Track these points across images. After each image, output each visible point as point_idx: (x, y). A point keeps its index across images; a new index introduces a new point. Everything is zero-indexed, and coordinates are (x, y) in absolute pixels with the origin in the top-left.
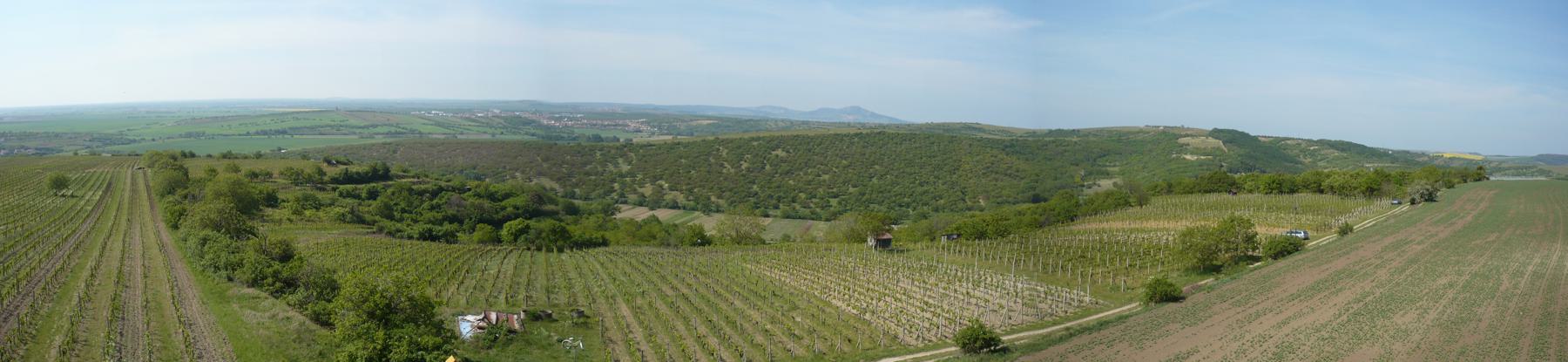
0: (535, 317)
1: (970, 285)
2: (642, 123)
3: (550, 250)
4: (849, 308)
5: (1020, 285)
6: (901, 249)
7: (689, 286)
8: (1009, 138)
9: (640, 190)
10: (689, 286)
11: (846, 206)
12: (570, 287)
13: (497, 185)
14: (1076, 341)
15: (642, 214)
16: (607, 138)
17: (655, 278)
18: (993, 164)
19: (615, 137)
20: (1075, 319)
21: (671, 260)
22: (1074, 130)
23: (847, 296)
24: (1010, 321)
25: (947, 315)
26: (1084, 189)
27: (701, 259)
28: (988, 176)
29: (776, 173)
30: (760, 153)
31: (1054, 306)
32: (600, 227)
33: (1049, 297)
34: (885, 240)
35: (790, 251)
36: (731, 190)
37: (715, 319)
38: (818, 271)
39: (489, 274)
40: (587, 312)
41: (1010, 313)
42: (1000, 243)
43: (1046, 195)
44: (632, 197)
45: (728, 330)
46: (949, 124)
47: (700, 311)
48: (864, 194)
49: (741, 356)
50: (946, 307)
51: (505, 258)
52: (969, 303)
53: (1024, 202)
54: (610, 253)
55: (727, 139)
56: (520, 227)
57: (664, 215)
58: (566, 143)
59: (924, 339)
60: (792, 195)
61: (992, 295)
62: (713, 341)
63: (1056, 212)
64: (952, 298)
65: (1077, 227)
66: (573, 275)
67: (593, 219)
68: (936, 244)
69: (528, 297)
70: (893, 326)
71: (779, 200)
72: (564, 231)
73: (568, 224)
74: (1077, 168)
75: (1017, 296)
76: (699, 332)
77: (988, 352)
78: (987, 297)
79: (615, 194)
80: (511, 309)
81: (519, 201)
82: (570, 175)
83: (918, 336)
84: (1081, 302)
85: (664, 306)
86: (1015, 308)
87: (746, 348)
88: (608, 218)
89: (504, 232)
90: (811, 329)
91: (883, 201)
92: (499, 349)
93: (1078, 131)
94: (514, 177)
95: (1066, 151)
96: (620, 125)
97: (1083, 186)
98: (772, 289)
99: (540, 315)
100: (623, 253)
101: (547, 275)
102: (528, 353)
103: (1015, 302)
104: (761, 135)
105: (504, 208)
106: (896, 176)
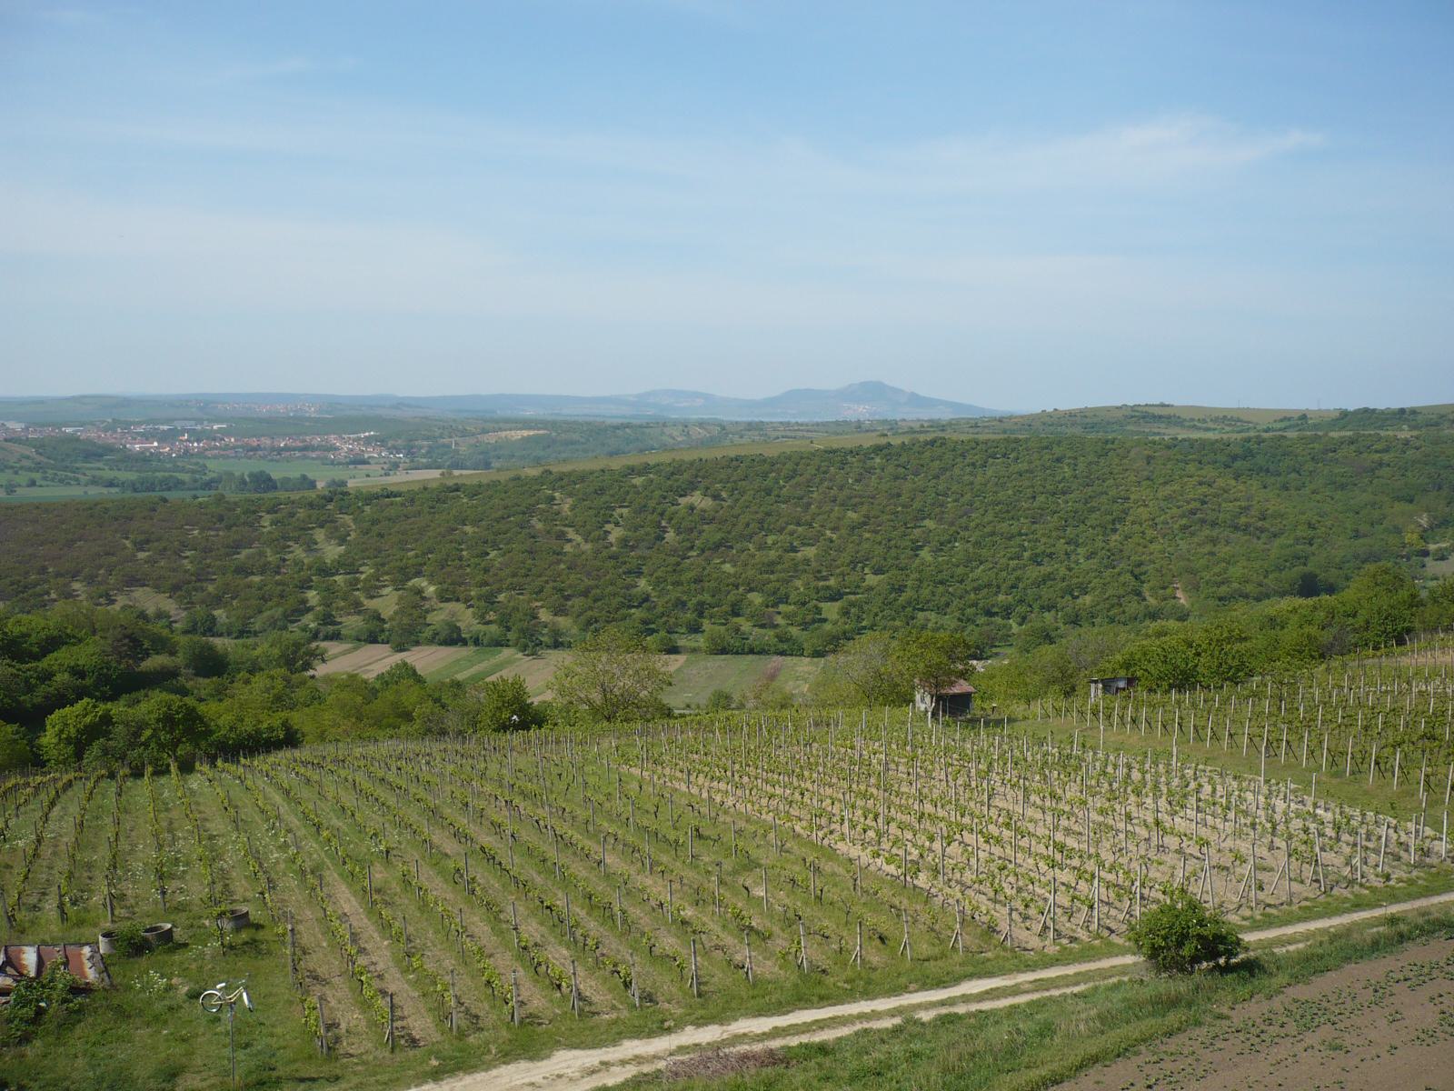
0: (135, 946)
1: (1163, 803)
2: (368, 441)
3: (161, 771)
4: (879, 861)
5: (1280, 805)
6: (995, 716)
7: (497, 826)
8: (1239, 436)
9: (370, 604)
10: (497, 826)
11: (859, 619)
12: (214, 856)
13: (24, 617)
14: (1414, 953)
15: (376, 662)
16: (287, 480)
17: (413, 815)
18: (1204, 503)
19: (304, 477)
20: (1411, 897)
21: (451, 768)
22: (1402, 411)
23: (871, 834)
24: (1261, 895)
25: (1111, 877)
26: (1428, 561)
27: (522, 762)
28: (1192, 534)
29: (692, 548)
30: (652, 504)
31: (1356, 861)
32: (279, 701)
33: (1345, 837)
34: (955, 696)
35: (731, 730)
36: (585, 594)
37: (560, 900)
38: (801, 777)
39: (13, 850)
40: (256, 915)
41: (1262, 876)
42: (1229, 698)
43: (1332, 575)
44: (352, 623)
45: (593, 926)
46: (1096, 411)
47: (523, 886)
48: (901, 589)
49: (627, 985)
50: (1108, 858)
51: (53, 804)
52: (1161, 848)
53: (1283, 594)
54: (305, 764)
55: (570, 474)
56: (88, 719)
57: (428, 660)
58: (187, 495)
59: (1058, 934)
60: (731, 598)
61: (1214, 828)
62: (558, 956)
63: (1360, 621)
64: (1122, 836)
65: (1414, 658)
66: (218, 825)
67: (259, 681)
68: (1077, 702)
69: (116, 899)
70: (984, 904)
71: (701, 610)
72: (192, 717)
73: (201, 700)
74: (1411, 507)
75: (1274, 833)
76: (525, 936)
77: (1211, 971)
78: (1204, 832)
79: (310, 616)
80: (75, 934)
81: (85, 654)
82: (201, 576)
83: (1045, 928)
84: (1426, 853)
85: (438, 880)
86: (1270, 862)
87: (638, 967)
88: (295, 678)
89: (48, 739)
90: (791, 914)
91: (947, 605)
92: (51, 1039)
93: (1414, 412)
94: (69, 595)
95: (1381, 464)
96: (313, 449)
97: (1426, 553)
98: (694, 823)
99: (145, 940)
100: (336, 761)
101: (156, 835)
102: (120, 1039)
103: (1271, 848)
104: (652, 460)
105: (47, 676)
106: (977, 544)
